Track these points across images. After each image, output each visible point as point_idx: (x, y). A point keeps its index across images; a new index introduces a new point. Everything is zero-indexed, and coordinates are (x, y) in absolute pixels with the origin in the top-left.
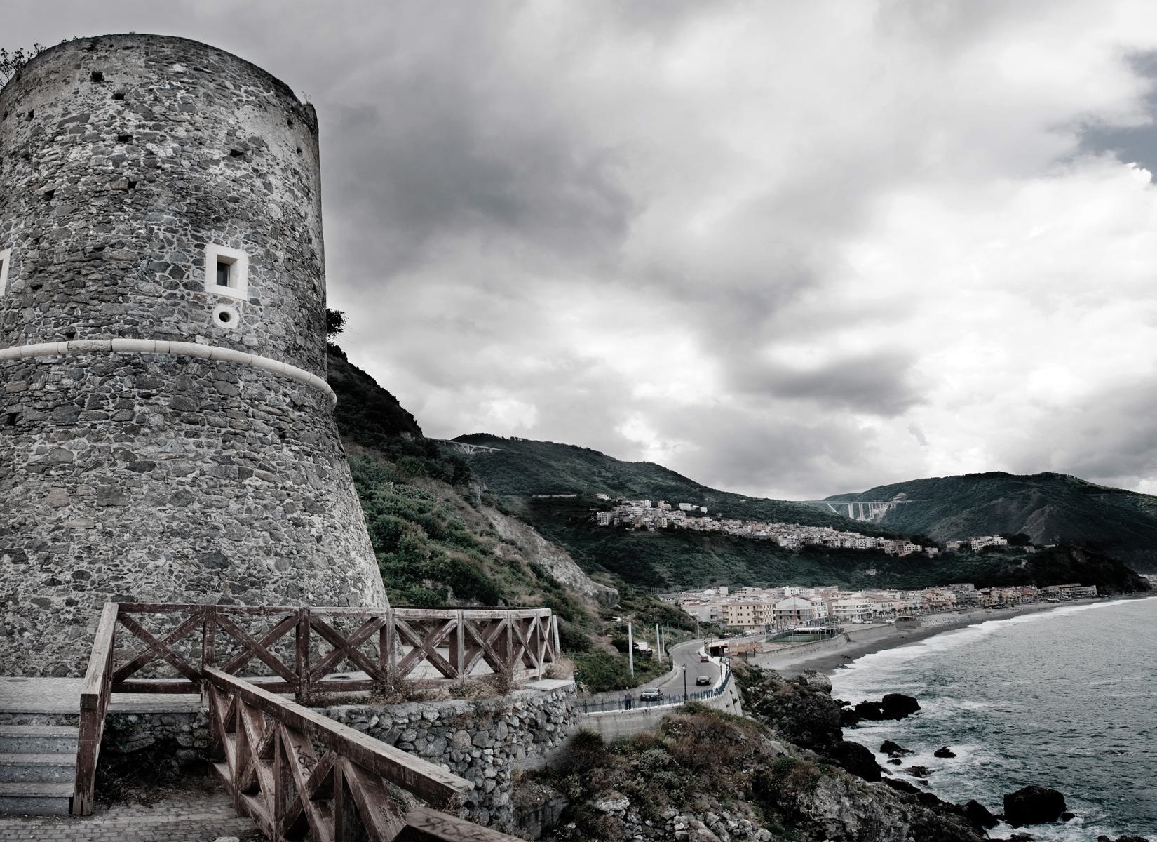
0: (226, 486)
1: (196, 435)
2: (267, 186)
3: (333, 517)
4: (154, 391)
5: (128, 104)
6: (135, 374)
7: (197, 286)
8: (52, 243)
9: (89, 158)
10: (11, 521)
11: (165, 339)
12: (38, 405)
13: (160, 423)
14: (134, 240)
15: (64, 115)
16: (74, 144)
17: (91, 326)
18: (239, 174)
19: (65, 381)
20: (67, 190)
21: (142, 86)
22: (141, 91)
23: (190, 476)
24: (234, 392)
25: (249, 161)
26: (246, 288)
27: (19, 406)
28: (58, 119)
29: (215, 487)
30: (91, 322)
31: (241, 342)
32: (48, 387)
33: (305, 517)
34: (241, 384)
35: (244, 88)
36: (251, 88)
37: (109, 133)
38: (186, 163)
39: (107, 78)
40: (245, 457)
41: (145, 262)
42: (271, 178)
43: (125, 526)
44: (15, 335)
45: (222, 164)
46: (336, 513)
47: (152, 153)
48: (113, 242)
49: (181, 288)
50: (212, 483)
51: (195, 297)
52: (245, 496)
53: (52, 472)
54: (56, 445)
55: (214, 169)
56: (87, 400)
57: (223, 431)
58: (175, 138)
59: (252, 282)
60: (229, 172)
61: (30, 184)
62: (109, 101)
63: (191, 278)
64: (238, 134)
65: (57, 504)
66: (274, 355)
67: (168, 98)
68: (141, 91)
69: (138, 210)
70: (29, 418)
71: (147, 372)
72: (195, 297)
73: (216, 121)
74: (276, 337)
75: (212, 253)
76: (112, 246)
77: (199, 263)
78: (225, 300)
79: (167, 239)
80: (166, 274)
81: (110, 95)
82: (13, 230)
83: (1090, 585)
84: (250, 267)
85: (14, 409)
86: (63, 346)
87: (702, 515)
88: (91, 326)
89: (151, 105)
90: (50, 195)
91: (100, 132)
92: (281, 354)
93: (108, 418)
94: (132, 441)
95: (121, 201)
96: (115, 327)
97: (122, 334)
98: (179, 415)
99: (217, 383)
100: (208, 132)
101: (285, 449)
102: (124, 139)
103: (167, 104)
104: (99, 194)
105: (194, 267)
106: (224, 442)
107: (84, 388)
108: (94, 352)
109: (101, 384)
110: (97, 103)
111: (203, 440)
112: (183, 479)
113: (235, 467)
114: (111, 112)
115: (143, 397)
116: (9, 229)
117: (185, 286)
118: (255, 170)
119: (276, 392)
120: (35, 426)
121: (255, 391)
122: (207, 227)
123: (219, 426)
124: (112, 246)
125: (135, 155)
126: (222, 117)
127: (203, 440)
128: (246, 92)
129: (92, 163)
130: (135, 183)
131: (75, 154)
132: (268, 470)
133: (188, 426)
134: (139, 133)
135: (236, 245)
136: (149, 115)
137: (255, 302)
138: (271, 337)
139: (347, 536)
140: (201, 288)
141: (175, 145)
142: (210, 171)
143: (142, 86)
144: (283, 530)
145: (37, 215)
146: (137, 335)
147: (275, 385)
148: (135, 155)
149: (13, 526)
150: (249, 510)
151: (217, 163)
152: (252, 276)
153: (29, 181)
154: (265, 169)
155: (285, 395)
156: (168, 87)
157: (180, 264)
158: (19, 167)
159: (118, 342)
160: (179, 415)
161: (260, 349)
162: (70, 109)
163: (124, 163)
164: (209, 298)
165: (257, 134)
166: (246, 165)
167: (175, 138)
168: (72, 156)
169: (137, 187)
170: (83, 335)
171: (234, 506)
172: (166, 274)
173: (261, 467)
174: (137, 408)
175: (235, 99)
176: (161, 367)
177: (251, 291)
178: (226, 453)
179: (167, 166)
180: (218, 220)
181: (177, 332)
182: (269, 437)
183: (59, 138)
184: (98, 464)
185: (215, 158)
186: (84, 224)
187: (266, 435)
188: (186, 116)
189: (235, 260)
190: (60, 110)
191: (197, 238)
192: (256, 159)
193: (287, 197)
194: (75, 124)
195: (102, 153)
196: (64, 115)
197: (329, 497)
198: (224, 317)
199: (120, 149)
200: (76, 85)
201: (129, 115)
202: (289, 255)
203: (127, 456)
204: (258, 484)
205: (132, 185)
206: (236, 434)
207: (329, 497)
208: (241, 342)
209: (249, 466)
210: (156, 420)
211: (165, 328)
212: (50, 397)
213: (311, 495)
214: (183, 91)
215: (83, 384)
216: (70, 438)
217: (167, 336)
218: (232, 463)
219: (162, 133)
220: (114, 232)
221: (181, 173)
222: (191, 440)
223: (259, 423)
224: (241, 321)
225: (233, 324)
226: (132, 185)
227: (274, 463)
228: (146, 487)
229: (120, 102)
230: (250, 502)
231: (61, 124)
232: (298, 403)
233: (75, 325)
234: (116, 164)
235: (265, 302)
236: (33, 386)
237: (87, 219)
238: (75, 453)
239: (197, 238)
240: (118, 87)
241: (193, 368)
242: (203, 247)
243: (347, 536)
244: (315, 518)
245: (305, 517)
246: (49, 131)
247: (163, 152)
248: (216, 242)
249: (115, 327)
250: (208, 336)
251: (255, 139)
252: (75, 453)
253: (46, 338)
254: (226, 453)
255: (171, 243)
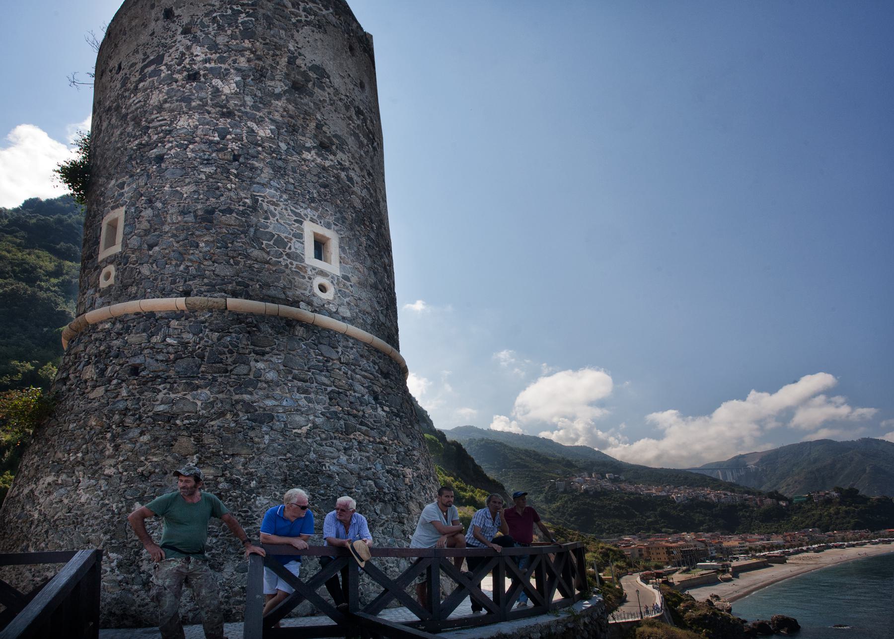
0: (335, 438)
1: (306, 392)
2: (350, 179)
3: (418, 469)
4: (268, 349)
5: (195, 37)
6: (249, 332)
7: (299, 258)
8: (164, 203)
9: (196, 127)
10: (140, 470)
11: (273, 302)
12: (160, 357)
13: (275, 379)
14: (241, 208)
15: (144, 60)
16: (153, 88)
17: (206, 285)
18: (327, 164)
19: (184, 336)
20: (177, 154)
21: (206, 15)
22: (206, 20)
23: (305, 429)
24: (335, 356)
25: (335, 155)
26: (338, 264)
27: (141, 357)
28: (139, 66)
29: (326, 439)
30: (206, 281)
31: (337, 312)
32: (169, 340)
33: (399, 468)
34: (340, 349)
35: (302, 5)
36: (311, 5)
37: (180, 72)
38: (283, 146)
39: (177, 12)
40: (349, 414)
41: (252, 230)
42: (352, 174)
43: (251, 474)
44: (133, 289)
45: (313, 152)
46: (420, 465)
47: (253, 131)
48: (223, 208)
49: (285, 257)
50: (323, 436)
51: (297, 267)
52: (351, 448)
53: (178, 422)
54: (180, 395)
55: (307, 155)
56: (207, 354)
57: (329, 389)
58: (273, 121)
59: (342, 261)
60: (319, 160)
61: (141, 146)
62: (179, 37)
63: (293, 249)
64: (324, 128)
65: (184, 452)
66: (363, 326)
67: (230, 25)
68: (206, 20)
69: (286, 209)
70: (151, 369)
71: (259, 330)
72: (297, 267)
73: (277, 47)
74: (365, 313)
75: (310, 229)
76: (222, 211)
77: (299, 236)
78: (322, 273)
79: (271, 212)
80: (271, 243)
81: (180, 30)
82: (126, 189)
83: (664, 409)
84: (340, 247)
85: (137, 360)
86: (180, 302)
87: (622, 481)
88: (206, 285)
89: (215, 36)
90: (160, 159)
91: (206, 104)
92: (369, 327)
93: (226, 371)
94: (251, 394)
95: (228, 171)
96: (230, 287)
97: (235, 295)
98: (291, 372)
99: (320, 346)
100: (269, 61)
101: (379, 409)
102: (193, 77)
103: (229, 32)
104: (208, 162)
105: (294, 240)
106: (330, 399)
107: (202, 342)
108: (210, 310)
109: (219, 339)
110: (169, 41)
111: (312, 396)
112: (299, 431)
113: (342, 422)
114: (182, 49)
115: (257, 353)
116: (123, 188)
117: (288, 255)
118: (340, 163)
119: (368, 360)
120: (159, 377)
121: (352, 357)
122: (304, 205)
123: (324, 384)
124: (222, 211)
125: (238, 131)
126: (282, 42)
127: (312, 396)
128: (305, 10)
129: (199, 132)
130: (239, 156)
131: (183, 122)
132: (367, 426)
133: (300, 384)
134: (206, 69)
135: (328, 226)
136: (214, 47)
137: (346, 278)
138: (360, 311)
139: (430, 486)
140: (302, 260)
141: (273, 127)
142: (304, 156)
143: (206, 15)
144: (384, 479)
145: (149, 177)
146: (248, 297)
147: (366, 354)
148: (238, 131)
149: (142, 475)
150: (355, 461)
151: (309, 150)
152: (343, 255)
153: (141, 144)
154: (347, 164)
155: (374, 363)
156: (229, 12)
157: (283, 235)
158: (130, 129)
159: (232, 302)
160: (291, 372)
161: (352, 321)
162: (149, 51)
163: (229, 137)
164: (309, 270)
165: (318, 63)
166: (332, 157)
167: (238, 70)
168: (180, 123)
169: (241, 160)
170: (199, 293)
171: (344, 458)
172: (271, 243)
173: (361, 424)
174: (252, 363)
175: (294, 20)
176: (272, 327)
177: (342, 268)
178: (333, 409)
179: (266, 144)
180: (313, 200)
181: (283, 296)
182: (366, 397)
183: (167, 105)
184: (222, 414)
185: (308, 145)
186: (194, 188)
187: (363, 396)
188: (247, 44)
189: (328, 239)
190: (140, 56)
191: (296, 214)
192: (340, 155)
193: (364, 193)
194: (153, 67)
195: (208, 124)
196: (144, 60)
197: (415, 453)
198: (323, 288)
199: (222, 123)
200: (152, 25)
201: (197, 50)
202: (369, 243)
203: (249, 407)
204: (361, 438)
205: (236, 158)
206: (339, 393)
207: (415, 453)
208: (337, 312)
209: (353, 421)
210: (271, 375)
211: (272, 292)
212: (171, 349)
213: (402, 450)
214: (244, 15)
215: (201, 339)
216: (193, 390)
217: (274, 300)
218: (339, 419)
219: (261, 114)
220: (222, 199)
221: (279, 153)
222: (303, 396)
223: (358, 387)
224: (336, 294)
225: (329, 295)
226: (236, 158)
227: (372, 420)
228: (267, 437)
229: (190, 36)
230: (356, 454)
231: (142, 69)
232: (385, 370)
233: (191, 283)
234: (223, 137)
235: (354, 279)
236: (154, 340)
237: (197, 183)
238: (199, 403)
239: (296, 214)
240: (186, 20)
241: (300, 331)
242: (301, 223)
243: (430, 486)
244: (408, 471)
245: (399, 468)
246: (133, 79)
247: (264, 132)
248: (312, 220)
249: (230, 287)
250: (310, 303)
251: (315, 68)
252: (199, 403)
253: (165, 294)
254: (333, 409)
255: (274, 216)
